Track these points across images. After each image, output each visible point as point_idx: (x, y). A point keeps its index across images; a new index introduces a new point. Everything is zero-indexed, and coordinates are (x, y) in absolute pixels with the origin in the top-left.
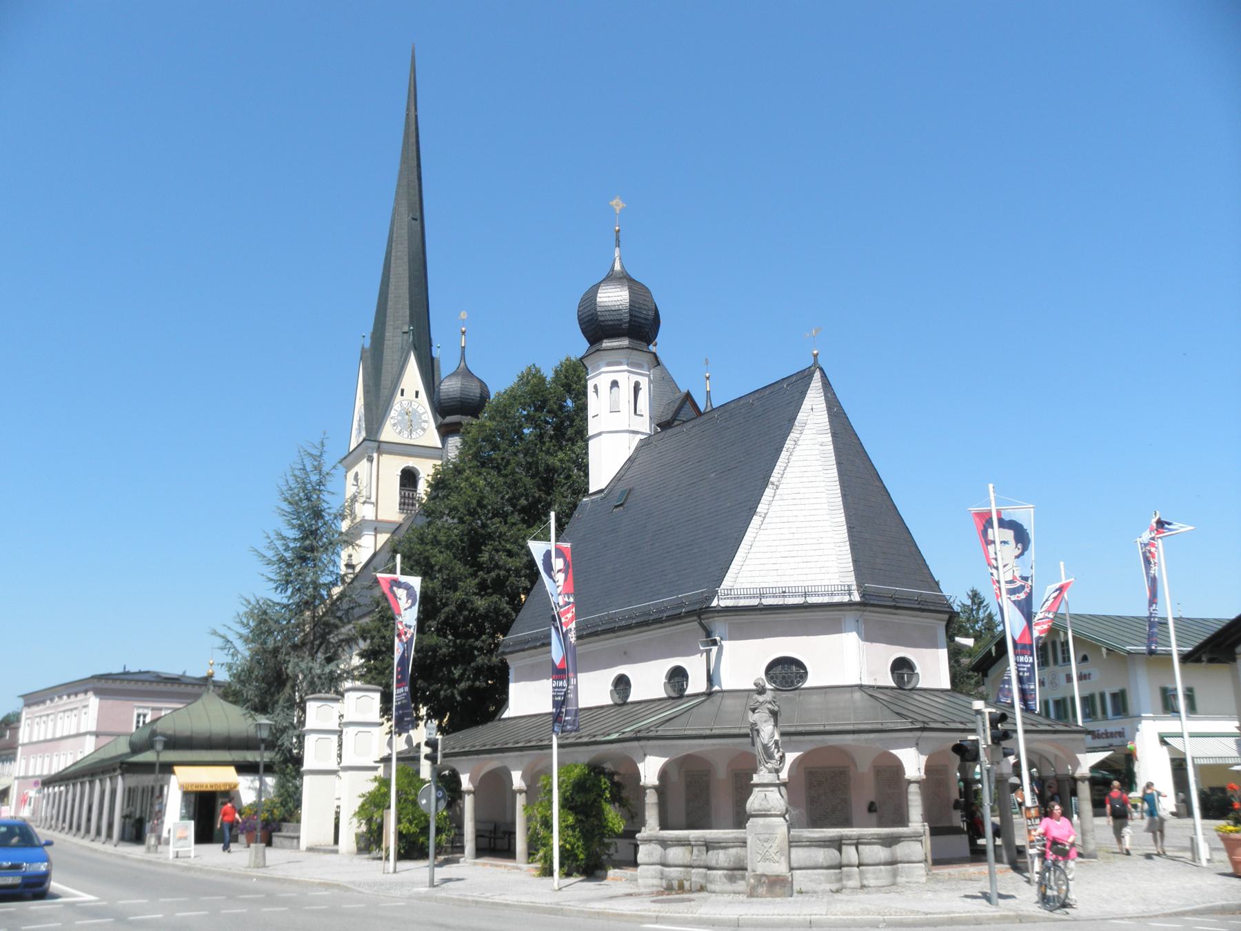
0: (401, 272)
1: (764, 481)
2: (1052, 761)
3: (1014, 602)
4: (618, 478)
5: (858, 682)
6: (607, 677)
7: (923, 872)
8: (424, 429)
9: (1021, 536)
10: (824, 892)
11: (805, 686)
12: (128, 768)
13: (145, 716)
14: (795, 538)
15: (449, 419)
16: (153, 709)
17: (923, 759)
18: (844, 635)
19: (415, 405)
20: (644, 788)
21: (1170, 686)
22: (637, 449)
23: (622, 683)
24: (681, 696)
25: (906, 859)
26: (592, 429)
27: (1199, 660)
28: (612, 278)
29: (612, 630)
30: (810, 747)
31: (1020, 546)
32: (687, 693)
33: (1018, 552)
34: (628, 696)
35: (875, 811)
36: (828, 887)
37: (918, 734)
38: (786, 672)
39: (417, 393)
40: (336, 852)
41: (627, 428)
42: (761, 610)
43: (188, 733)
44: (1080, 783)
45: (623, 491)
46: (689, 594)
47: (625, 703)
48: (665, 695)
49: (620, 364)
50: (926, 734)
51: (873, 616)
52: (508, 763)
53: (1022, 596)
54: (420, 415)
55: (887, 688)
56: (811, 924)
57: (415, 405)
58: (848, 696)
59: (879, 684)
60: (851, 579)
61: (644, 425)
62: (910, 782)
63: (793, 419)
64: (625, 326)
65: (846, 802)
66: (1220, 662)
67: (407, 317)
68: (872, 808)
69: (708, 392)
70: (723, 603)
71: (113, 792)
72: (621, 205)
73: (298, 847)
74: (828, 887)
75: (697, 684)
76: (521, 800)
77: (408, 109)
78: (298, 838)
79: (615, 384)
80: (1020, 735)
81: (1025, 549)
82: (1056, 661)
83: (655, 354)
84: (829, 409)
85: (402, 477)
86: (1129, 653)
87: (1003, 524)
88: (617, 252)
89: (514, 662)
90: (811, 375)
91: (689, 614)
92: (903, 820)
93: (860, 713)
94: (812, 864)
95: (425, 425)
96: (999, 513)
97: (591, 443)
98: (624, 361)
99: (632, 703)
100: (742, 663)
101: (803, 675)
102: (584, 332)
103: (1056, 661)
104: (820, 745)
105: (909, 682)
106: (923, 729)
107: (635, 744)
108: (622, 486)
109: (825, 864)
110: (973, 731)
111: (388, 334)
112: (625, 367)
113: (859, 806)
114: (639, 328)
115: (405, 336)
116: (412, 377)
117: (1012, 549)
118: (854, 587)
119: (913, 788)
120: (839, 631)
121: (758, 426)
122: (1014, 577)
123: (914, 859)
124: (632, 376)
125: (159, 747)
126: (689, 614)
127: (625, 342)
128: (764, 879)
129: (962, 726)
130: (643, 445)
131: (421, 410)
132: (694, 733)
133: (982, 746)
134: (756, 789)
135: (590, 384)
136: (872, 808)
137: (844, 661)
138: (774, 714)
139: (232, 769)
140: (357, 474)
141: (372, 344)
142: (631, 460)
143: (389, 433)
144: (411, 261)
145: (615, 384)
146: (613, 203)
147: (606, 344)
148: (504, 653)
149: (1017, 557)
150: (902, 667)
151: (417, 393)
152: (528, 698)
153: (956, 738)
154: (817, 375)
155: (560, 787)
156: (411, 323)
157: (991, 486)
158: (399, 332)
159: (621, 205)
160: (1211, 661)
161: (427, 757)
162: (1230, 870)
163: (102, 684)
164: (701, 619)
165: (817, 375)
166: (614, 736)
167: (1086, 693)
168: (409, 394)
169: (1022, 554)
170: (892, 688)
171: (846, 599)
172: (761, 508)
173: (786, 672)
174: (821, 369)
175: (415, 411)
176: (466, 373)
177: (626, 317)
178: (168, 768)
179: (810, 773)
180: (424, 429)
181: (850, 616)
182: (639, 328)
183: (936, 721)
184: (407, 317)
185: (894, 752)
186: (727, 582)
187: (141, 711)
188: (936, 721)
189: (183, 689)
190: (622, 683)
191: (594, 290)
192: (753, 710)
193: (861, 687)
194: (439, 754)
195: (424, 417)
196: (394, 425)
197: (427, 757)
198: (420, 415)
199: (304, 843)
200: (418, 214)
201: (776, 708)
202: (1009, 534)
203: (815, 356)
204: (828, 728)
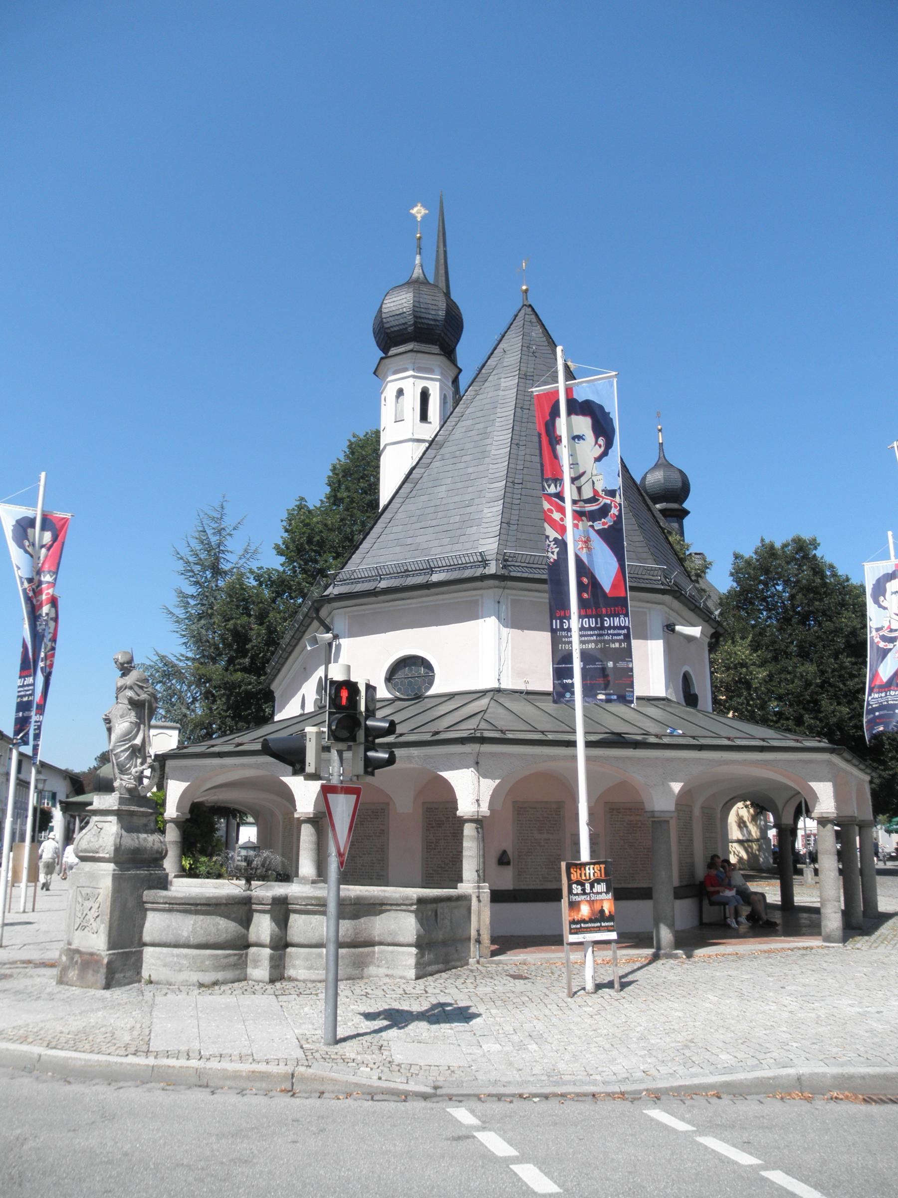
3: (598, 532)
5: (495, 685)
7: (412, 961)
9: (603, 428)
10: (186, 984)
17: (489, 786)
18: (481, 621)
20: (462, 821)
25: (389, 940)
31: (601, 441)
33: (598, 451)
35: (508, 863)
36: (196, 977)
41: (410, 436)
49: (406, 370)
53: (608, 521)
59: (531, 687)
62: (300, 822)
64: (410, 329)
69: (661, 445)
72: (424, 211)
74: (196, 977)
77: (438, 247)
79: (400, 392)
81: (609, 444)
87: (576, 407)
88: (418, 257)
94: (170, 938)
96: (569, 391)
98: (410, 366)
101: (430, 680)
102: (379, 346)
109: (192, 941)
112: (411, 373)
117: (590, 448)
119: (469, 830)
120: (476, 617)
122: (596, 492)
123: (401, 939)
124: (418, 381)
127: (410, 346)
128: (77, 957)
134: (94, 819)
146: (414, 211)
149: (598, 459)
159: (424, 211)
169: (605, 454)
173: (411, 671)
177: (410, 320)
179: (612, 810)
181: (488, 595)
185: (441, 773)
202: (583, 424)
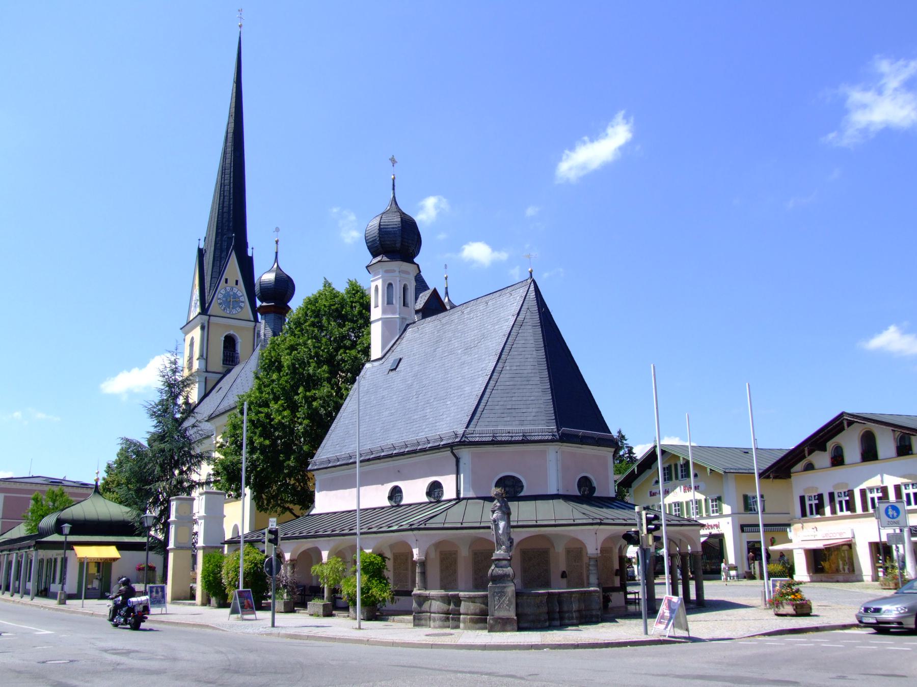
2: (678, 543)
6: (423, 484)
8: (241, 307)
19: (235, 290)
21: (750, 494)
23: (395, 493)
24: (439, 502)
27: (768, 477)
37: (596, 527)
39: (237, 282)
47: (399, 506)
50: (602, 527)
52: (411, 542)
54: (239, 297)
57: (235, 290)
66: (781, 478)
68: (564, 575)
80: (663, 527)
82: (677, 478)
85: (225, 341)
89: (319, 477)
95: (242, 305)
103: (677, 478)
104: (528, 535)
106: (600, 524)
107: (410, 533)
113: (555, 575)
129: (624, 522)
131: (239, 294)
140: (192, 339)
151: (237, 282)
152: (327, 502)
153: (624, 529)
155: (204, 577)
160: (775, 478)
161: (270, 541)
162: (794, 612)
168: (232, 282)
175: (235, 294)
180: (241, 307)
190: (395, 493)
195: (242, 299)
196: (220, 304)
198: (239, 297)
204: (539, 523)
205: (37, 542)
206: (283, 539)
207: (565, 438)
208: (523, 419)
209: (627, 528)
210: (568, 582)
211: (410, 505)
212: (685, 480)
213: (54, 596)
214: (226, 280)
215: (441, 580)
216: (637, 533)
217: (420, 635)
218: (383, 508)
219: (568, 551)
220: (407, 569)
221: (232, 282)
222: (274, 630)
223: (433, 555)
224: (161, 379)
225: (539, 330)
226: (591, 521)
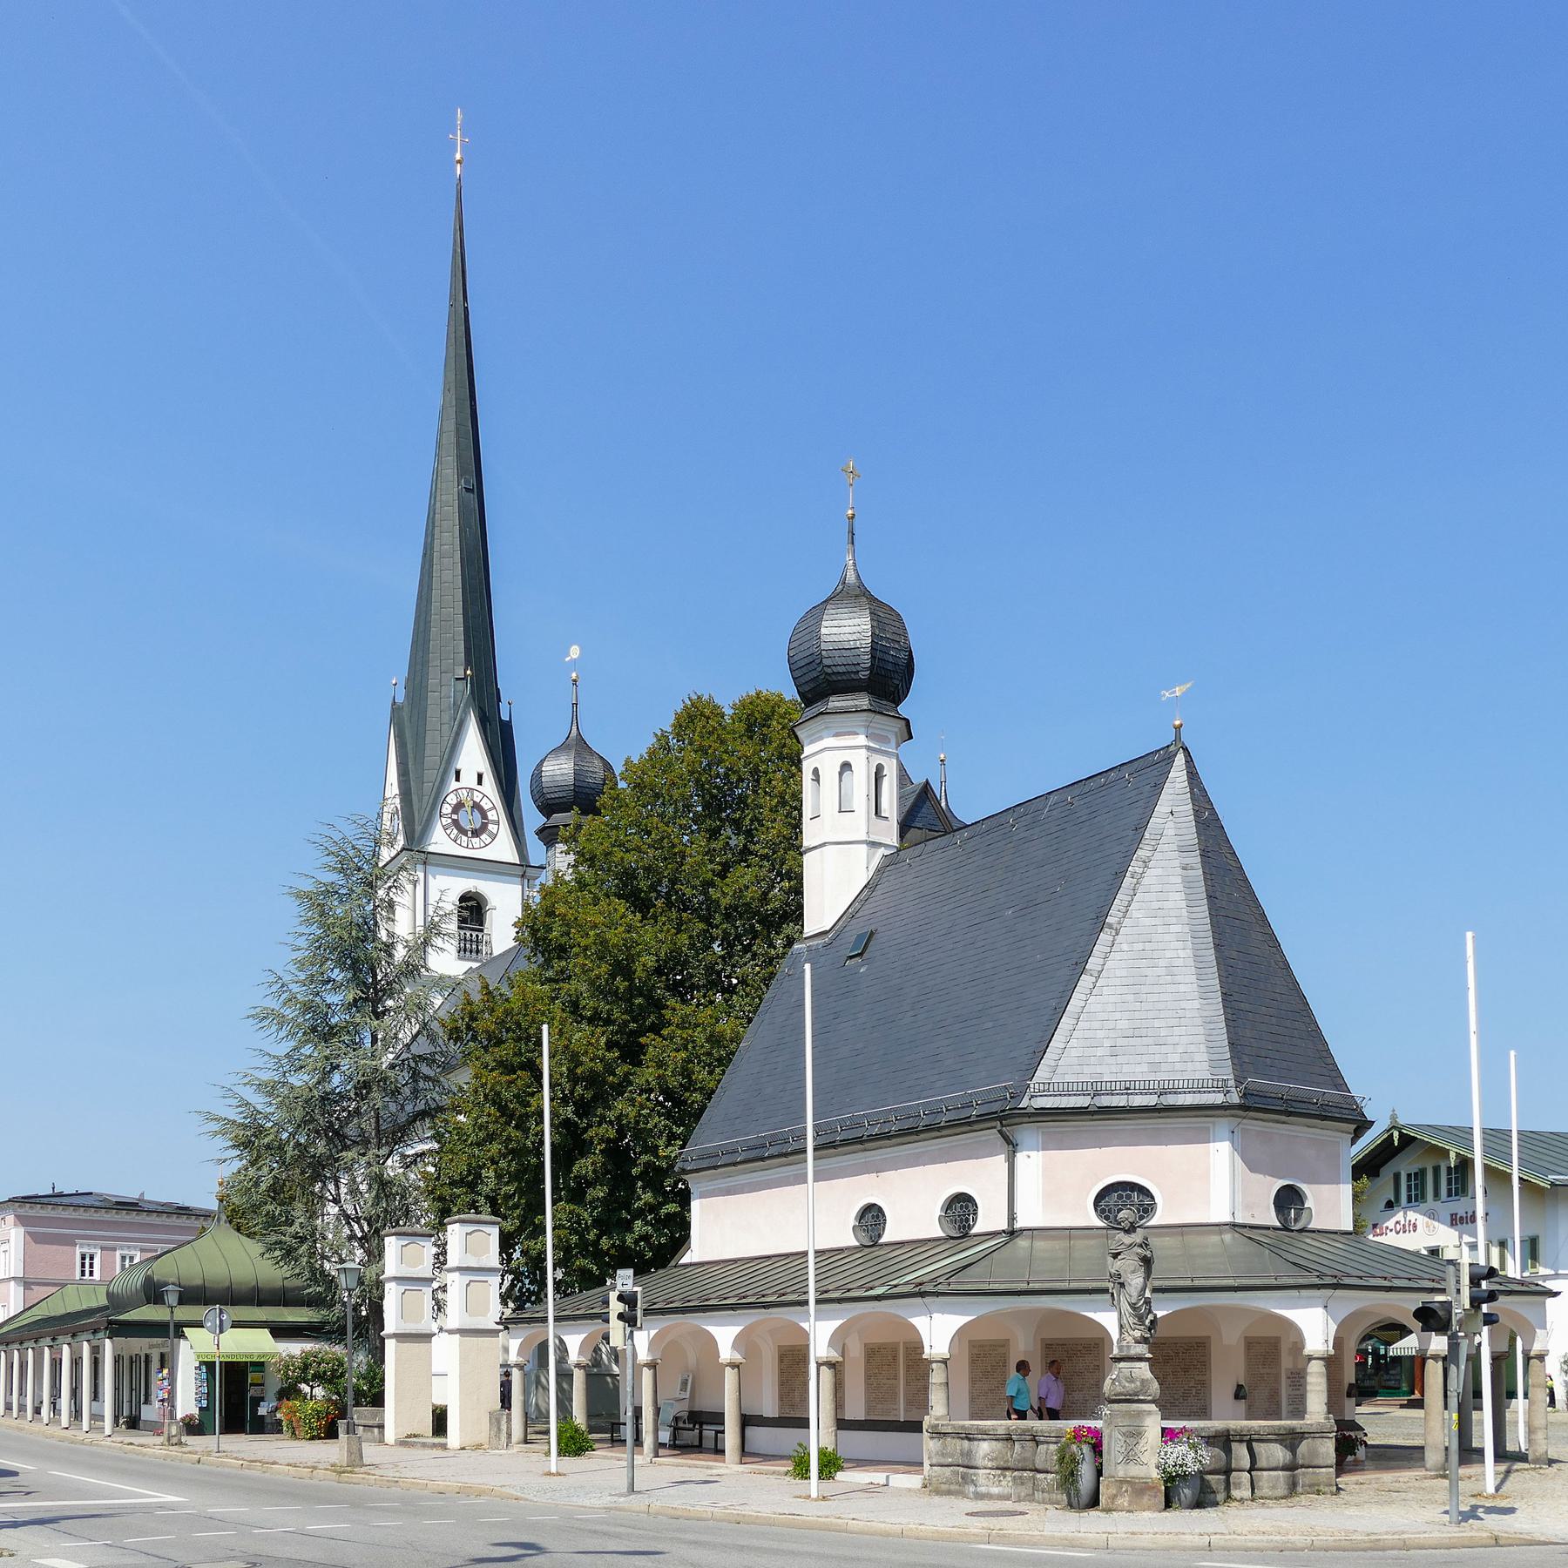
0: (450, 574)
1: (1099, 923)
4: (850, 915)
11: (1152, 1222)
12: (121, 1330)
13: (132, 1258)
14: (1142, 1001)
15: (558, 818)
16: (142, 1250)
22: (879, 871)
23: (872, 1217)
26: (809, 837)
28: (854, 594)
29: (859, 1140)
30: (1352, 1308)
32: (973, 1231)
34: (880, 1236)
35: (1244, 1397)
37: (1329, 1292)
38: (1123, 1201)
39: (480, 777)
40: (444, 1447)
42: (1159, 1111)
43: (199, 1282)
44: (1430, 1362)
45: (858, 937)
46: (983, 1088)
48: (941, 1234)
51: (1254, 1126)
55: (1268, 1228)
56: (1377, 1546)
58: (1215, 1239)
60: (1227, 1073)
61: (889, 834)
62: (1310, 1358)
63: (1140, 828)
64: (864, 675)
65: (1204, 1386)
67: (466, 655)
70: (1040, 1103)
71: (76, 1363)
73: (381, 1441)
75: (989, 1219)
76: (730, 1376)
78: (381, 1427)
79: (846, 766)
82: (1437, 1194)
83: (907, 721)
84: (1197, 814)
86: (1552, 1184)
89: (695, 1183)
90: (1170, 759)
91: (984, 1118)
92: (1299, 1411)
93: (1215, 1259)
97: (806, 858)
99: (887, 1244)
100: (1046, 1188)
101: (1148, 1209)
105: (1296, 1220)
108: (859, 928)
110: (1443, 1291)
111: (432, 682)
114: (884, 679)
115: (461, 684)
116: (473, 755)
118: (1232, 1083)
121: (1085, 831)
125: (172, 1299)
126: (984, 1118)
127: (863, 701)
130: (889, 864)
131: (486, 805)
132: (1003, 1287)
133: (1457, 1311)
135: (807, 767)
136: (1239, 1393)
137: (1206, 1184)
138: (1147, 1262)
139: (265, 1334)
141: (407, 696)
142: (870, 886)
143: (440, 840)
144: (466, 562)
145: (846, 766)
147: (835, 702)
148: (684, 1171)
150: (1288, 1199)
151: (480, 777)
154: (1180, 759)
156: (468, 663)
157: (1469, 935)
158: (448, 678)
161: (621, 1317)
163: (27, 1210)
164: (1005, 1121)
165: (1180, 759)
166: (879, 1291)
167: (1531, 1233)
168: (468, 779)
170: (1275, 1229)
171: (1218, 1099)
172: (1093, 963)
173: (1123, 1201)
174: (1186, 750)
176: (578, 746)
177: (866, 660)
178: (178, 1330)
181: (1223, 1124)
182: (884, 679)
183: (1349, 1276)
184: (466, 655)
186: (1042, 1074)
187: (85, 1250)
188: (1349, 1276)
189: (143, 1218)
190: (872, 1217)
191: (816, 614)
192: (1115, 1256)
193: (1234, 1225)
194: (639, 1313)
197: (621, 1317)
199: (390, 1435)
200: (473, 481)
201: (1148, 1254)
203: (1178, 728)
204: (1197, 1283)
205: (110, 1322)
206: (646, 1312)
207: (1253, 1105)
208: (1157, 1058)
209: (1427, 1297)
210: (1249, 1407)
211: (902, 1244)
212: (1459, 1206)
213: (155, 1428)
214: (458, 773)
215: (972, 1400)
216: (1447, 1306)
217: (948, 1518)
218: (841, 1250)
219: (1250, 1343)
220: (896, 1377)
221: (468, 779)
222: (634, 1502)
223: (856, 1351)
224: (218, 1189)
225: (1195, 859)
226: (1317, 1281)
